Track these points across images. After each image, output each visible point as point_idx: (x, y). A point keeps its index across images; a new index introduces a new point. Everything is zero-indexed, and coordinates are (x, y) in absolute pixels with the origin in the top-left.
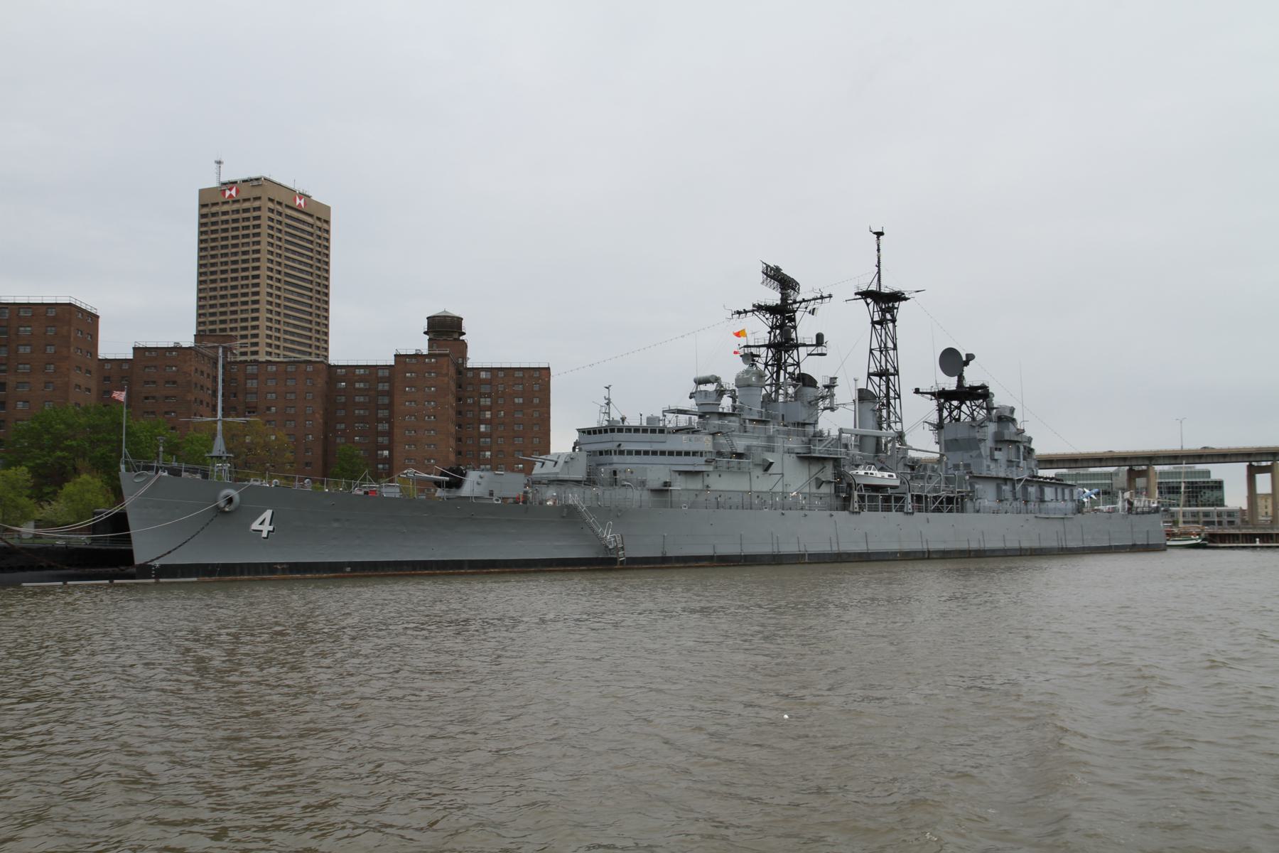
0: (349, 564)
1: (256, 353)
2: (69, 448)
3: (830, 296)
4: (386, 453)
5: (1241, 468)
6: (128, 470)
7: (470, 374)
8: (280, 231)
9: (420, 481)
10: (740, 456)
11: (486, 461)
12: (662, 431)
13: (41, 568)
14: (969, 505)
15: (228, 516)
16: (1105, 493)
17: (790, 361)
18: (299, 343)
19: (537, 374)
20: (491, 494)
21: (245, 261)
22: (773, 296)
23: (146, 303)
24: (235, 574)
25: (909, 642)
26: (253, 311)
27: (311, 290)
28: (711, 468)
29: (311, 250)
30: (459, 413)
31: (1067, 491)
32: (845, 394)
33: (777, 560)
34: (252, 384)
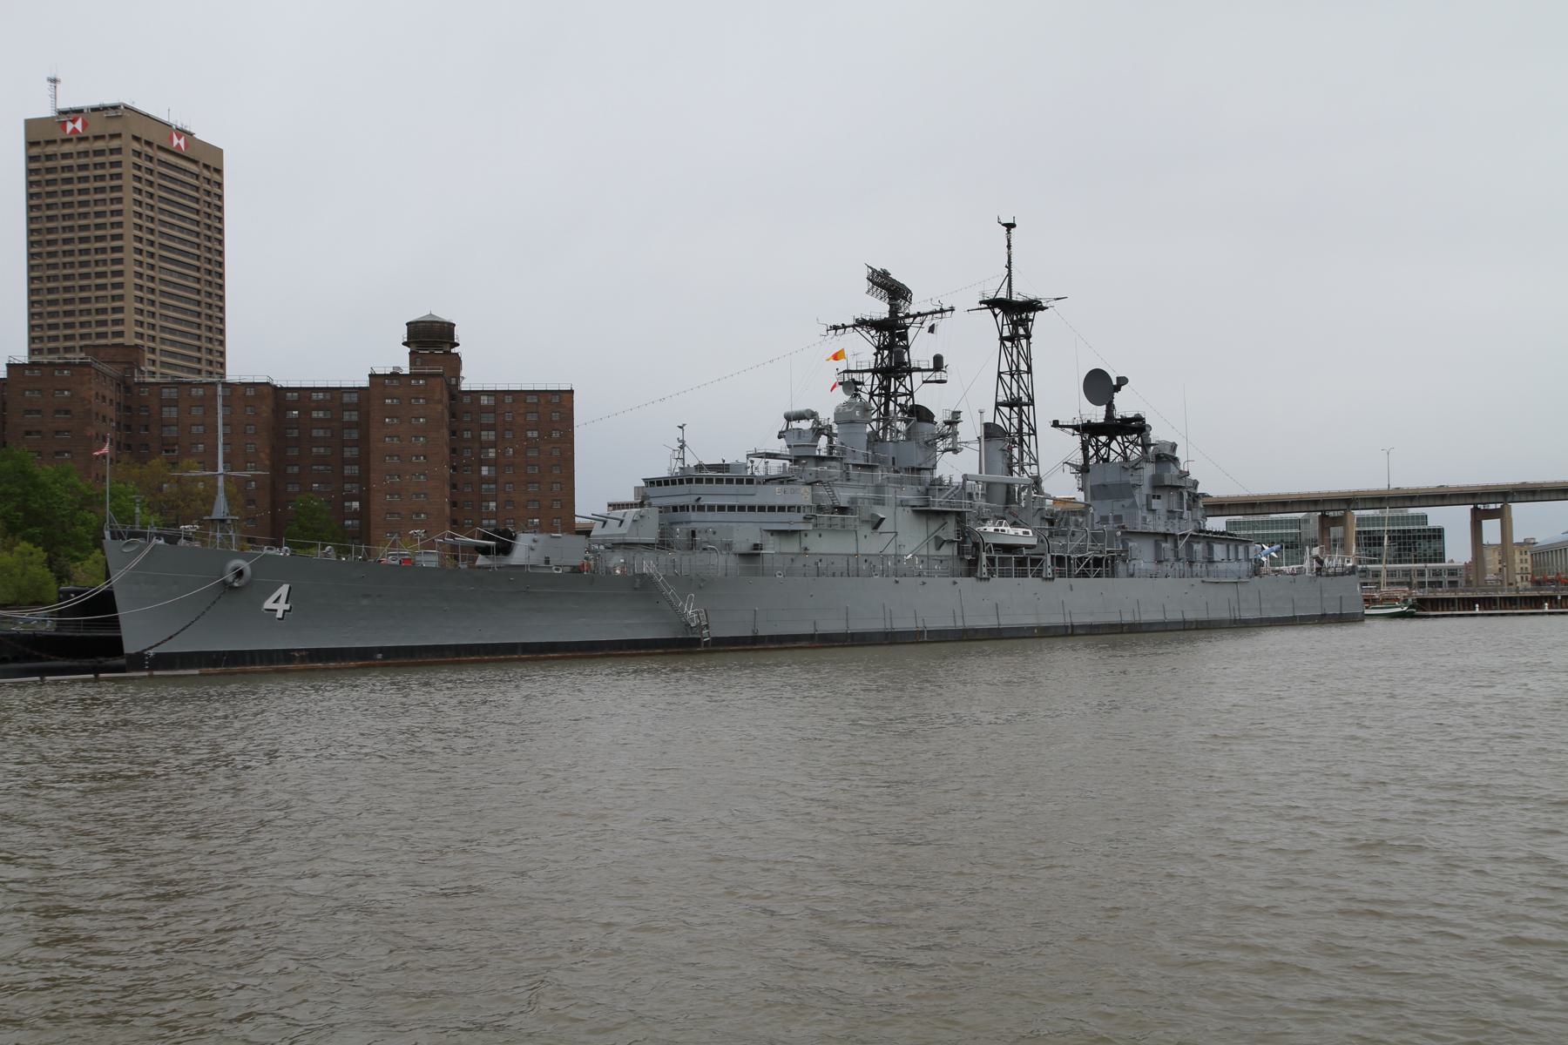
0: (381, 650)
3: (952, 309)
4: (356, 505)
5: (1465, 511)
6: (113, 538)
7: (467, 400)
8: (151, 184)
10: (843, 510)
12: (750, 481)
14: (1121, 567)
17: (902, 390)
19: (556, 399)
20: (547, 562)
24: (244, 664)
28: (810, 527)
29: (198, 212)
30: (453, 451)
31: (1241, 548)
32: (970, 430)
33: (890, 638)
34: (170, 413)
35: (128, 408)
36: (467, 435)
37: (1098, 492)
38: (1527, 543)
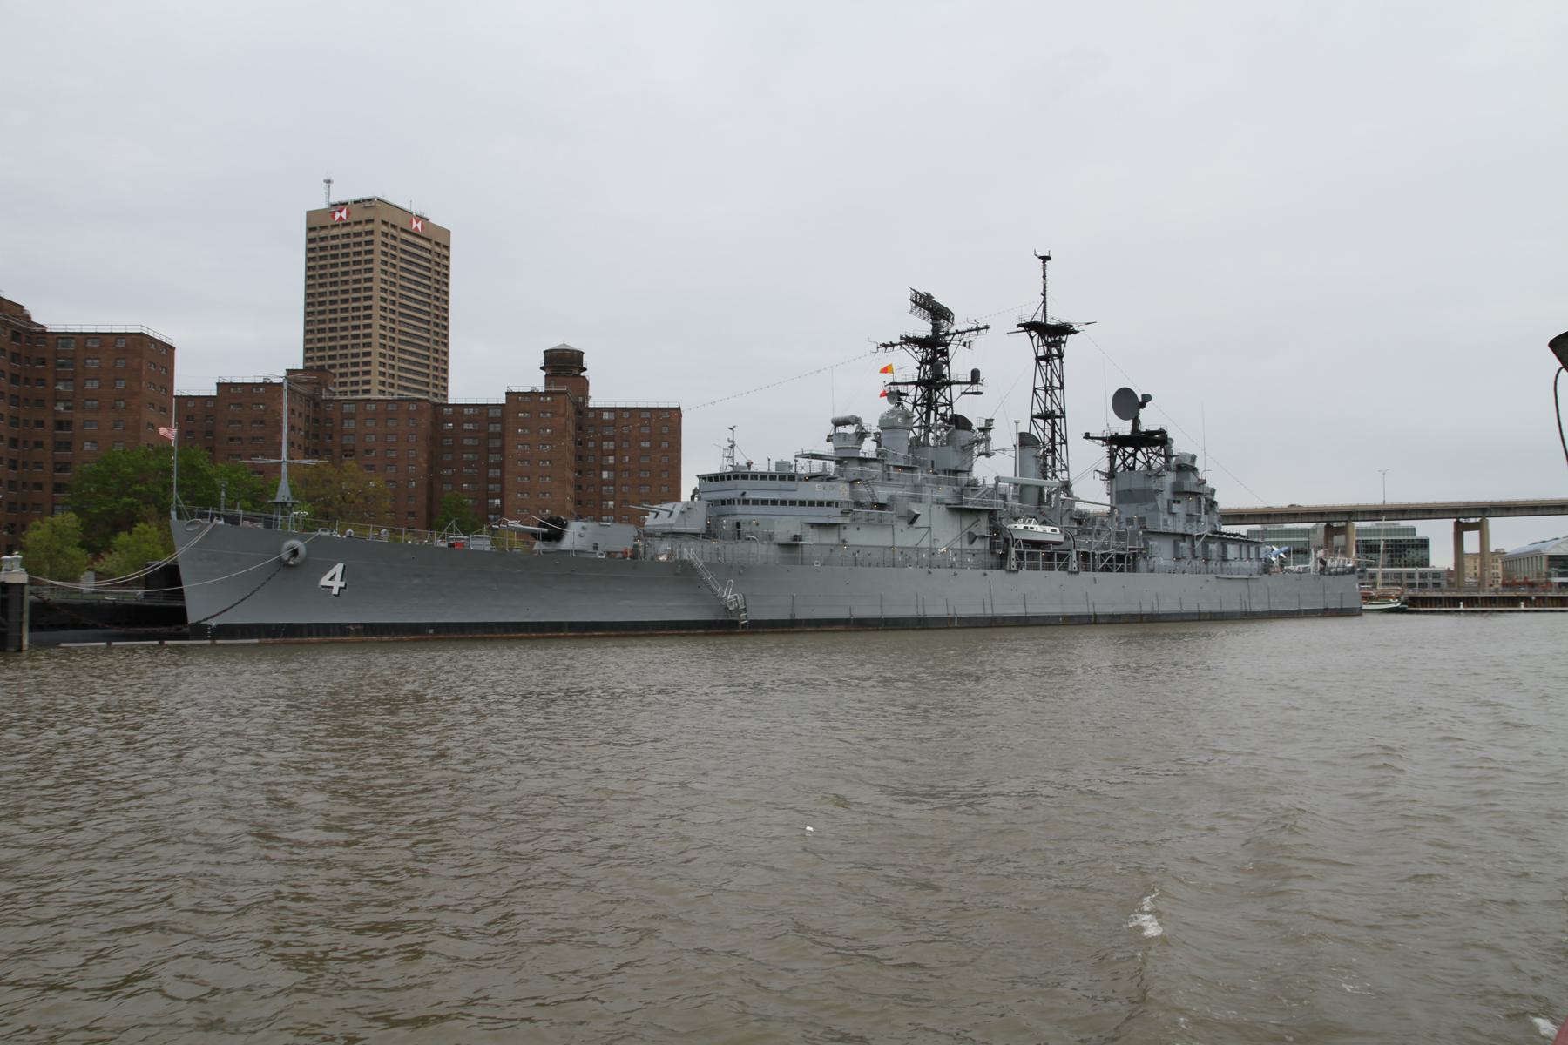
0: (432, 625)
1: (368, 391)
2: (137, 494)
4: (497, 502)
5: (1448, 525)
6: (179, 517)
7: (591, 415)
9: (521, 533)
10: (882, 506)
11: (609, 512)
12: (792, 478)
13: (85, 627)
14: (1142, 563)
15: (293, 571)
16: (1296, 552)
17: (942, 400)
18: (416, 381)
20: (596, 547)
21: (355, 291)
22: (923, 328)
23: (237, 329)
24: (301, 635)
25: (1070, 722)
26: (365, 345)
27: (428, 323)
28: (847, 521)
29: (429, 278)
30: (579, 458)
31: (1252, 549)
32: (1004, 437)
34: (349, 425)
35: (316, 420)
36: (591, 444)
37: (1121, 497)
38: (1497, 552)
